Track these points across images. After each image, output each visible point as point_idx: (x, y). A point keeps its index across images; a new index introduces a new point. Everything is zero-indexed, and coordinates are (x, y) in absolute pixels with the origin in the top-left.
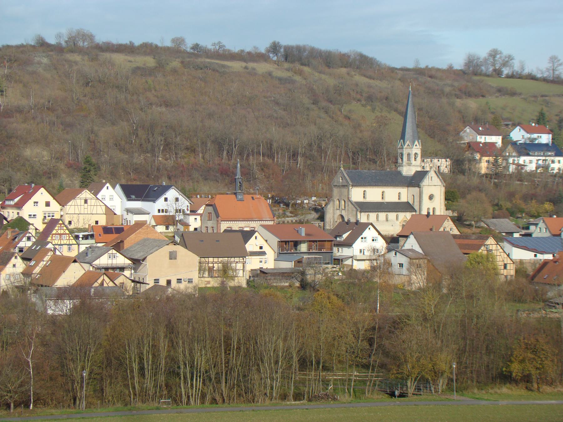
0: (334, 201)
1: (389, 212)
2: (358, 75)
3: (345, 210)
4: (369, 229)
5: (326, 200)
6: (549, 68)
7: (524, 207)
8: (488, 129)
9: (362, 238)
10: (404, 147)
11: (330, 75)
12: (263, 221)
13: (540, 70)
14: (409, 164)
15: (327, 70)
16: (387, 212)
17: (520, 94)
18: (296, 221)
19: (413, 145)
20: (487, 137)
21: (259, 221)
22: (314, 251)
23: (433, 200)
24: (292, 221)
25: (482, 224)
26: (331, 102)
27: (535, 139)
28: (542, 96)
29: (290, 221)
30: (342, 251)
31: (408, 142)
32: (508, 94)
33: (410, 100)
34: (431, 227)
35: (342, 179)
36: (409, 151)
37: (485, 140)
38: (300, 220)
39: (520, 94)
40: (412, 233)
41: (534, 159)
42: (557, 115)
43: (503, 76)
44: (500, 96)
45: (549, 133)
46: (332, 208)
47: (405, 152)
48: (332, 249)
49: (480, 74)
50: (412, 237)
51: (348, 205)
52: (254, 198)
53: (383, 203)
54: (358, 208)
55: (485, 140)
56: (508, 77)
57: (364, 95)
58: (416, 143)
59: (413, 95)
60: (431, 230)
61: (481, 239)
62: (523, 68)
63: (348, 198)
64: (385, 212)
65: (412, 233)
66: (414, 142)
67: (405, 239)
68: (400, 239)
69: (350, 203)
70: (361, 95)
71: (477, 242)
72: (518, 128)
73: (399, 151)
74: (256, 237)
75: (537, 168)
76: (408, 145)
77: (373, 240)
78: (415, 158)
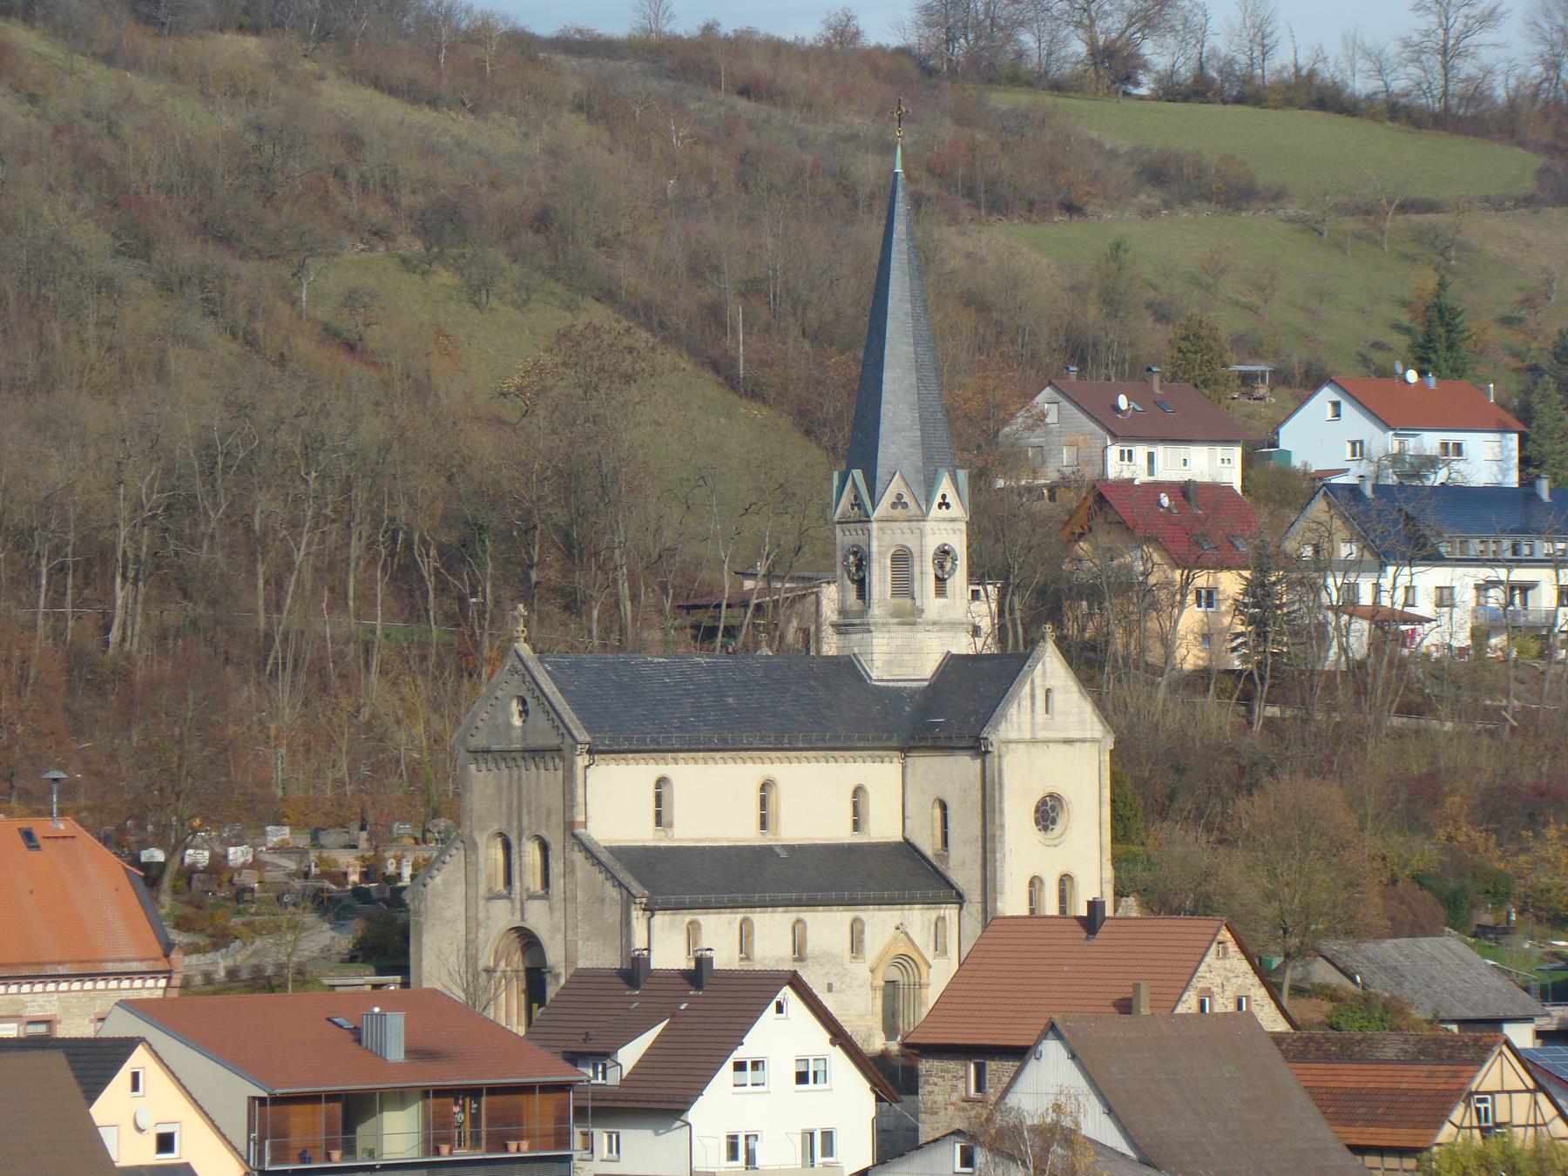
0: (471, 846)
1: (812, 903)
2: (331, 75)
3: (546, 896)
4: (780, 1009)
5: (363, 844)
6: (1416, 38)
7: (1501, 866)
8: (1159, 404)
9: (740, 1066)
10: (875, 515)
11: (174, 72)
12: (105, 976)
13: (1367, 54)
14: (909, 617)
15: (148, 45)
16: (799, 903)
17: (1278, 196)
18: (232, 973)
19: (929, 501)
20: (1161, 451)
21: (81, 977)
22: (462, 1154)
23: (1058, 828)
24: (208, 978)
25: (1322, 973)
26: (226, 240)
27: (1431, 463)
28: (1404, 208)
29: (199, 979)
30: (616, 1147)
31: (896, 486)
32: (1207, 197)
33: (900, 229)
34: (1127, 992)
35: (524, 713)
36: (900, 535)
37: (1151, 472)
38: (257, 971)
39: (1278, 196)
40: (1052, 1027)
41: (1464, 580)
42: (1506, 321)
43: (1143, 91)
44: (1167, 204)
45: (1503, 429)
46: (460, 889)
47: (881, 542)
48: (563, 1140)
49: (1017, 78)
50: (1052, 1050)
51: (569, 870)
52: (38, 834)
53: (769, 849)
54: (636, 888)
55: (1151, 472)
56: (1172, 92)
57: (407, 200)
58: (945, 486)
59: (917, 201)
60: (1125, 1006)
61: (1439, 1060)
62: (1262, 41)
63: (569, 826)
64: (787, 904)
65: (1052, 1029)
66: (930, 485)
67: (1010, 1066)
68: (924, 1065)
69: (578, 857)
70: (393, 203)
71: (1415, 1077)
72: (1326, 395)
73: (844, 538)
74: (135, 1077)
75: (1480, 635)
76: (899, 502)
77: (802, 1078)
78: (940, 581)
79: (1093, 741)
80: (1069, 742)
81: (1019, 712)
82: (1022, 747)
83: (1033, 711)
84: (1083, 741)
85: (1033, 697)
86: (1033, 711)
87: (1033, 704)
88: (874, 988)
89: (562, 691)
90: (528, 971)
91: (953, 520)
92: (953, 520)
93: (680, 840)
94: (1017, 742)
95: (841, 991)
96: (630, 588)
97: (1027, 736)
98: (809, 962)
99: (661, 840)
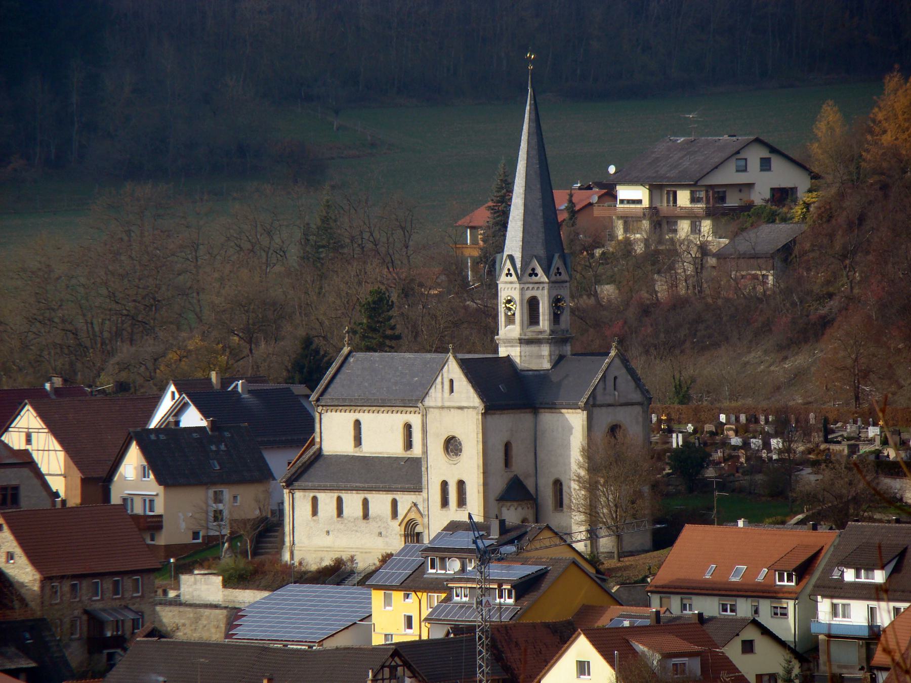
1: (370, 490)
79: (474, 408)
81: (436, 391)
82: (437, 411)
83: (443, 391)
85: (442, 383)
86: (443, 391)
87: (443, 387)
88: (400, 535)
91: (511, 283)
92: (511, 283)
93: (365, 453)
94: (433, 408)
95: (387, 537)
97: (440, 404)
98: (370, 520)
99: (356, 452)
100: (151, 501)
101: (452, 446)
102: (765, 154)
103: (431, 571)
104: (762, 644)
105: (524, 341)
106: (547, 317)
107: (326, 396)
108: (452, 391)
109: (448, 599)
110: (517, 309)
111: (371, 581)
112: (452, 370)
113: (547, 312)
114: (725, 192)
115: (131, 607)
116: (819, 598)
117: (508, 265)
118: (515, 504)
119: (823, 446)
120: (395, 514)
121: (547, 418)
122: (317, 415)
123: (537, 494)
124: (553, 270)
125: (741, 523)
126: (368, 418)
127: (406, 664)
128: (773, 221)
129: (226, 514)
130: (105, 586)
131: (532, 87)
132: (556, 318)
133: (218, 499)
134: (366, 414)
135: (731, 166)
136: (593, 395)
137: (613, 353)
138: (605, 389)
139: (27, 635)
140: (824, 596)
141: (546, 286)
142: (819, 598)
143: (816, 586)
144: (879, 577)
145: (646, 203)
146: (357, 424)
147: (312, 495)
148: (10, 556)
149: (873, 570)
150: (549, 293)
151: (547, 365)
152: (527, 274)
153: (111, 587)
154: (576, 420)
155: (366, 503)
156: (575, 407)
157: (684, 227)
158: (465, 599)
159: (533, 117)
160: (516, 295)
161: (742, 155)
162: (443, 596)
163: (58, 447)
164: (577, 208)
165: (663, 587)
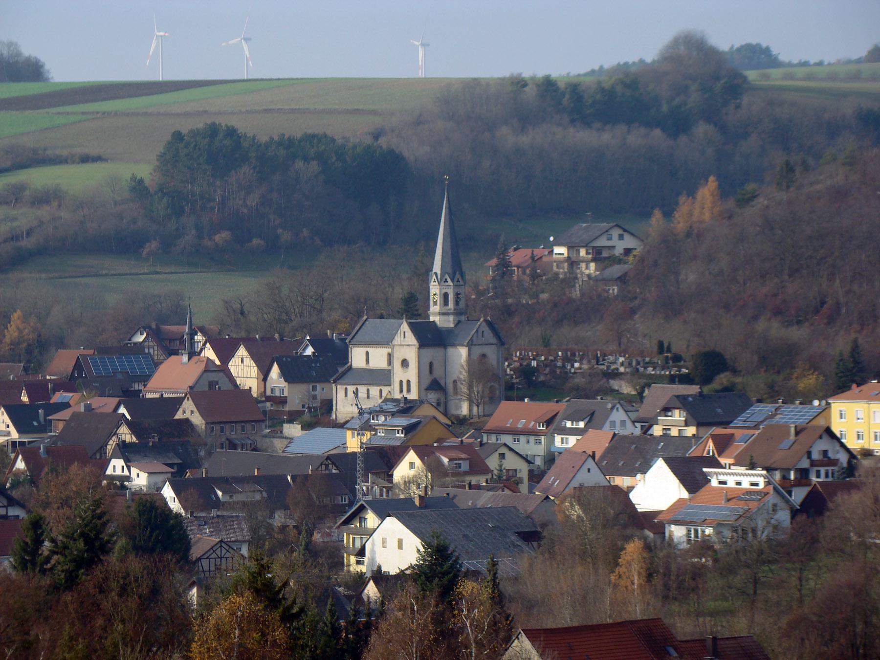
79: (414, 345)
80: (408, 345)
84: (412, 345)
89: (434, 252)
90: (457, 389)
92: (436, 285)
96: (150, 533)
100: (283, 390)
101: (405, 363)
102: (621, 232)
103: (372, 421)
104: (509, 455)
105: (441, 314)
106: (452, 302)
107: (354, 340)
108: (404, 337)
109: (376, 434)
110: (437, 298)
111: (347, 426)
112: (405, 327)
113: (452, 299)
114: (601, 250)
115: (250, 438)
116: (556, 435)
117: (434, 277)
118: (434, 391)
119: (596, 366)
120: (381, 396)
121: (450, 350)
122: (350, 349)
123: (446, 387)
124: (456, 279)
125: (526, 400)
126: (371, 350)
127: (333, 463)
128: (620, 264)
129: (319, 397)
130: (237, 427)
131: (447, 192)
132: (457, 302)
133: (314, 388)
134: (371, 349)
135: (604, 238)
136: (471, 340)
137: (482, 320)
138: (477, 337)
139: (180, 448)
140: (558, 434)
141: (452, 287)
142: (556, 435)
143: (555, 430)
144: (582, 425)
145: (566, 255)
146: (367, 353)
147: (345, 387)
148: (192, 412)
149: (579, 421)
150: (453, 290)
151: (452, 325)
152: (443, 281)
153: (240, 428)
154: (463, 352)
155: (368, 390)
156: (463, 345)
157: (583, 265)
158: (383, 435)
159: (447, 206)
160: (438, 292)
161: (610, 232)
162: (374, 433)
163: (254, 365)
164: (536, 258)
165: (489, 430)
